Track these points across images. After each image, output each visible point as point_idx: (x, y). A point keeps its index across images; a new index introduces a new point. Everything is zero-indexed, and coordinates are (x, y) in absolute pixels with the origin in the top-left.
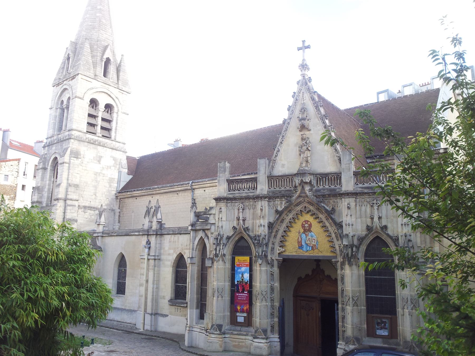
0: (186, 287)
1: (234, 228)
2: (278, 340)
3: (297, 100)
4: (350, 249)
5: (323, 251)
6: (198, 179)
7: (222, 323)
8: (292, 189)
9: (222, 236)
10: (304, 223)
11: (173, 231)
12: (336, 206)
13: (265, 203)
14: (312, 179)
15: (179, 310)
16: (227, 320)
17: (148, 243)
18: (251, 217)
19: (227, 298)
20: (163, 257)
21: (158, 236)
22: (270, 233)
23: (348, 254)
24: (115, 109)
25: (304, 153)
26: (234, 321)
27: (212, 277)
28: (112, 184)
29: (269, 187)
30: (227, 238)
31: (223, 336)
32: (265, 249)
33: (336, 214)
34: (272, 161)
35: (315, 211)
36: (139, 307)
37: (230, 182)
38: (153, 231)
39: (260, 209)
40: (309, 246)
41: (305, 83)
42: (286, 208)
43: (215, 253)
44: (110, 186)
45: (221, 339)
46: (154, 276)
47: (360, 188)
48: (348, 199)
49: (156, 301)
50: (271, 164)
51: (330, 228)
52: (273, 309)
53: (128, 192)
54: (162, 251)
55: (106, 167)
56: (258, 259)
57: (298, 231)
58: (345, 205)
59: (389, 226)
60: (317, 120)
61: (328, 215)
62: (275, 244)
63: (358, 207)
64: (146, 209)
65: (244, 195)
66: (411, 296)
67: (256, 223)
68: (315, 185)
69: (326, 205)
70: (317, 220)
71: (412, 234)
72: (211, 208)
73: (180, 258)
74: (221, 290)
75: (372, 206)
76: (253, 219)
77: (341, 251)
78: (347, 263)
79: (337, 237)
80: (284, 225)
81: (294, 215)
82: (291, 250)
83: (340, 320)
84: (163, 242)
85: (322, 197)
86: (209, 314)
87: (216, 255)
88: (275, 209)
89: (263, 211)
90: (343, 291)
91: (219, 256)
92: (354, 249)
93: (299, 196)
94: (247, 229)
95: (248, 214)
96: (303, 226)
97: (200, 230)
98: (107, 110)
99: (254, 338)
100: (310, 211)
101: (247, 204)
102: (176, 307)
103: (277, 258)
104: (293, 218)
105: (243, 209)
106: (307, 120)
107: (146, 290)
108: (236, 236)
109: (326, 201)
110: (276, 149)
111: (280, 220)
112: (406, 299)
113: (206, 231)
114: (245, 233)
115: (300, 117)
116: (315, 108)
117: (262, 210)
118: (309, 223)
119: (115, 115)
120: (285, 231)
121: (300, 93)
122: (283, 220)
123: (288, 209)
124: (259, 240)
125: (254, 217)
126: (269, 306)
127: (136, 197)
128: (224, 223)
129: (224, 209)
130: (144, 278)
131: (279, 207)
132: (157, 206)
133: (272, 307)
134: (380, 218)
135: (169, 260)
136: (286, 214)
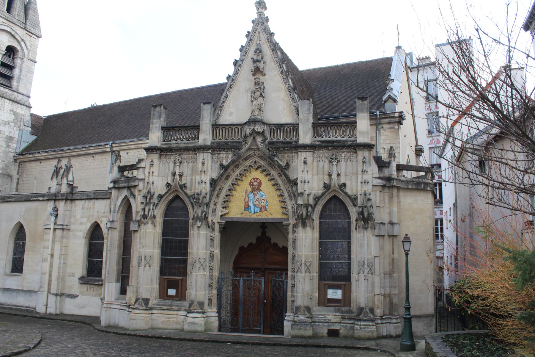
0: (102, 262)
1: (168, 185)
2: (217, 315)
3: (251, 40)
4: (305, 209)
5: (274, 212)
6: (120, 139)
7: (148, 297)
8: (241, 140)
9: (152, 194)
10: (253, 181)
11: (87, 195)
12: (291, 161)
13: (207, 156)
14: (266, 129)
17: (56, 209)
18: (190, 172)
20: (72, 227)
22: (213, 191)
23: (302, 215)
24: (20, 54)
25: (257, 99)
26: (163, 295)
28: (10, 144)
29: (213, 137)
30: (158, 196)
31: (150, 312)
32: (205, 209)
33: (291, 169)
34: (217, 108)
35: (267, 167)
36: (41, 287)
37: (165, 129)
38: (63, 195)
40: (258, 208)
41: (261, 23)
42: (233, 162)
43: (143, 213)
44: (8, 146)
45: (147, 315)
46: (61, 250)
47: (318, 141)
48: (305, 153)
49: (62, 279)
50: (217, 111)
51: (282, 187)
52: (212, 279)
53: (30, 154)
54: (72, 220)
55: (4, 122)
56: (196, 221)
57: (245, 190)
58: (301, 160)
59: (348, 184)
60: (273, 64)
63: (315, 163)
64: (54, 169)
66: (368, 259)
67: (195, 179)
68: (268, 136)
69: (280, 160)
70: (269, 177)
71: (372, 193)
73: (96, 227)
74: (149, 259)
75: (331, 162)
76: (192, 174)
77: (294, 212)
78: (300, 225)
79: (290, 196)
80: (229, 182)
81: (241, 171)
82: (236, 211)
84: (73, 209)
85: (276, 148)
86: (133, 286)
87: (145, 217)
88: (219, 163)
89: (206, 165)
91: (148, 217)
92: (310, 209)
93: (250, 149)
95: (186, 168)
96: (251, 184)
97: (124, 188)
98: (8, 54)
99: (188, 313)
101: (186, 156)
102: (89, 286)
103: (219, 221)
105: (181, 163)
106: (262, 62)
107: (51, 266)
108: (170, 195)
109: (280, 156)
110: (224, 94)
111: (225, 176)
112: (362, 262)
113: (132, 190)
114: (181, 191)
115: (255, 58)
117: (203, 163)
118: (258, 181)
119: (18, 61)
121: (255, 33)
122: (229, 176)
123: (234, 164)
124: (199, 199)
125: (194, 171)
127: (40, 160)
129: (156, 162)
131: (224, 161)
133: (211, 277)
134: (339, 175)
135: (81, 231)
136: (233, 169)
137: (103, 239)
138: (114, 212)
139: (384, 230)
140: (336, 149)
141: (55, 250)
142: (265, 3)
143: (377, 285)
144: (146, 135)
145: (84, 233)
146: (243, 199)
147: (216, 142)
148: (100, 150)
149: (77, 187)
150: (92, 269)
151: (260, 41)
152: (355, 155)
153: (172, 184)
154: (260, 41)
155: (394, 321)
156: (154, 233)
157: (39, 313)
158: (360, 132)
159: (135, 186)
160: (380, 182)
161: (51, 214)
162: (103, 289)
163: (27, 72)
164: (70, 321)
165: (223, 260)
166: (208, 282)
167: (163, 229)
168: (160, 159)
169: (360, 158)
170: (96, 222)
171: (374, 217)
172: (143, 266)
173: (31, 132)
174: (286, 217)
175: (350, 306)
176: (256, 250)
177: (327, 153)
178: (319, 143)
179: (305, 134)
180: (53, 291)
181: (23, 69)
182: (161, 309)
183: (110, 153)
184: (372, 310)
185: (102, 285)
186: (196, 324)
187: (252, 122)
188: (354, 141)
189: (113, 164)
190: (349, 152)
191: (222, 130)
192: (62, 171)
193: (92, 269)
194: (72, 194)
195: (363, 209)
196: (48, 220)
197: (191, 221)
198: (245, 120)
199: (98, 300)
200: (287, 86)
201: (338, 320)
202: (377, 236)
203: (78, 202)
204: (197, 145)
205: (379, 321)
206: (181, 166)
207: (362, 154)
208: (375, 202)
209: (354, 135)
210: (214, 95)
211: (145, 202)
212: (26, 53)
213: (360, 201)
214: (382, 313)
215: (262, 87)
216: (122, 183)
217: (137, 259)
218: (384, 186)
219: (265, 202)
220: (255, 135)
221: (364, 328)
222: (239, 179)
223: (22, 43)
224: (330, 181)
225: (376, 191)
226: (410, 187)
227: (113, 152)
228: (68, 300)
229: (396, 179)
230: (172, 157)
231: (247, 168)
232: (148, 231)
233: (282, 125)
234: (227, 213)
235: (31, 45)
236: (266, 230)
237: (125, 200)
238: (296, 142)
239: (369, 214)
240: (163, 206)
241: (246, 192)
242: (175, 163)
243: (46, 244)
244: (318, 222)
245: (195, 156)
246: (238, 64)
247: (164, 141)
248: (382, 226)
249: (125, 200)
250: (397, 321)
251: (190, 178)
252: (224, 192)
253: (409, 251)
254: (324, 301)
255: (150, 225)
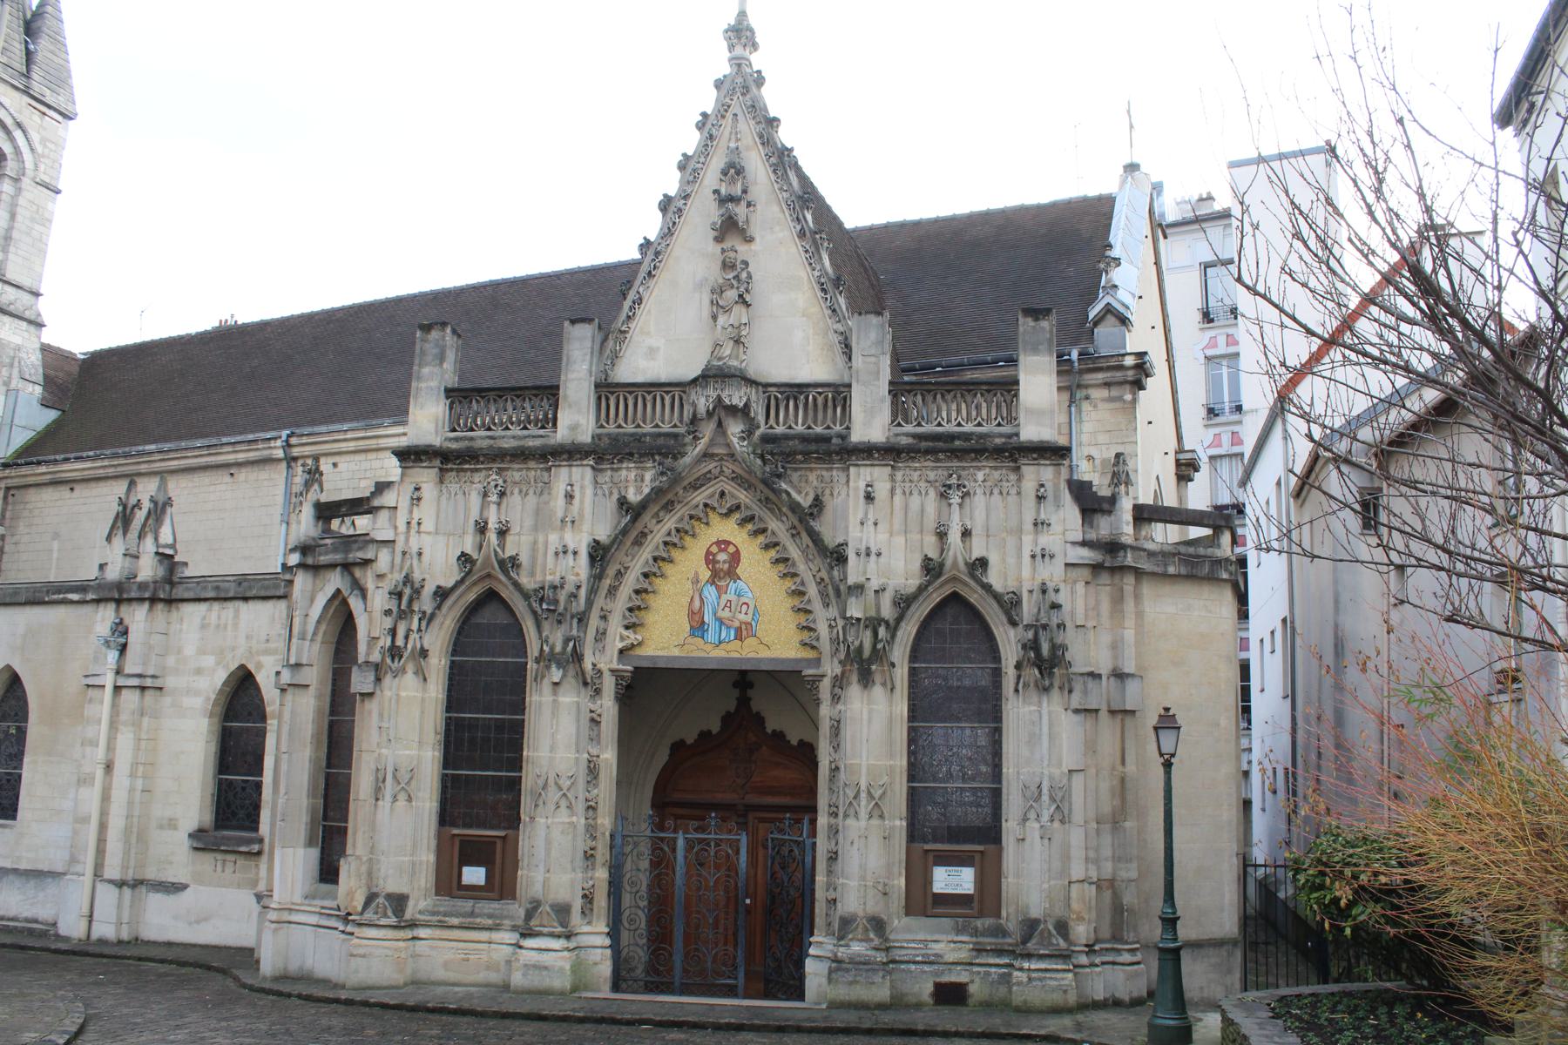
0: (258, 786)
1: (464, 558)
2: (608, 942)
3: (711, 137)
4: (869, 633)
5: (776, 640)
6: (313, 423)
7: (404, 890)
8: (682, 430)
9: (417, 585)
10: (714, 549)
11: (217, 588)
12: (827, 492)
13: (580, 475)
14: (753, 397)
15: (230, 866)
16: (425, 878)
17: (121, 629)
18: (529, 522)
19: (428, 805)
20: (170, 682)
21: (160, 606)
22: (597, 577)
23: (860, 649)
26: (448, 884)
27: (374, 732)
30: (435, 593)
32: (574, 632)
34: (611, 336)
35: (757, 510)
36: (73, 860)
37: (456, 395)
38: (143, 586)
39: (562, 493)
40: (728, 627)
41: (741, 90)
42: (657, 492)
43: (389, 643)
46: (137, 749)
47: (907, 435)
48: (869, 469)
50: (610, 343)
51: (801, 567)
53: (39, 463)
54: (171, 661)
56: (548, 667)
57: (691, 576)
58: (856, 489)
59: (994, 559)
60: (776, 208)
61: (801, 521)
62: (610, 618)
64: (115, 508)
65: (507, 444)
66: (1051, 778)
68: (761, 418)
69: (794, 487)
70: (761, 539)
71: (1062, 586)
72: (381, 487)
73: (242, 687)
75: (943, 496)
76: (535, 528)
77: (835, 641)
78: (854, 678)
79: (823, 595)
80: (646, 553)
82: (666, 639)
83: (821, 866)
85: (783, 454)
86: (359, 858)
87: (395, 652)
88: (616, 496)
89: (576, 501)
90: (835, 770)
91: (406, 655)
92: (882, 632)
93: (706, 455)
94: (510, 565)
95: (518, 510)
96: (710, 559)
97: (333, 566)
99: (524, 936)
100: (738, 507)
101: (517, 476)
102: (219, 856)
103: (615, 666)
104: (678, 531)
105: (502, 494)
106: (744, 204)
107: (106, 797)
109: (795, 476)
110: (632, 295)
112: (1034, 788)
113: (358, 573)
116: (770, 171)
117: (569, 497)
118: (731, 549)
120: (646, 575)
122: (644, 535)
123: (662, 499)
124: (556, 602)
125: (541, 521)
126: (581, 829)
127: (71, 483)
128: (427, 542)
129: (429, 491)
130: (100, 753)
132: (161, 499)
134: (966, 534)
135: (197, 693)
136: (657, 514)
137: (263, 718)
138: (303, 638)
139: (1098, 695)
140: (960, 459)
141: (118, 751)
142: (752, 31)
143: (1077, 853)
144: (399, 412)
145: (208, 699)
146: (685, 601)
147: (608, 435)
148: (252, 455)
149: (186, 564)
150: (228, 805)
151: (738, 140)
152: (1013, 477)
153: (475, 557)
154: (738, 140)
155: (1127, 957)
156: (423, 700)
157: (67, 939)
158: (1030, 411)
159: (366, 563)
160: (1086, 555)
161: (107, 642)
162: (263, 867)
163: (33, 220)
164: (162, 961)
165: (625, 780)
166: (582, 846)
167: (449, 690)
168: (441, 482)
169: (1029, 485)
170: (242, 667)
171: (1068, 656)
172: (388, 798)
173: (43, 398)
174: (811, 654)
175: (998, 916)
176: (722, 754)
177: (933, 468)
178: (910, 440)
179: (870, 413)
180: (112, 871)
181: (19, 210)
182: (443, 926)
183: (284, 464)
184: (1062, 928)
185: (259, 853)
186: (546, 968)
187: (715, 376)
188: (1010, 436)
189: (292, 503)
190: (996, 468)
191: (626, 399)
192: (140, 516)
193: (228, 805)
194: (172, 584)
195: (1036, 634)
196: (96, 659)
197: (531, 666)
198: (694, 371)
199: (246, 898)
200: (817, 273)
201: (963, 955)
202: (1077, 711)
203: (188, 609)
204: (552, 442)
205: (1084, 960)
206: (504, 505)
207: (1036, 474)
208: (1073, 613)
209: (1012, 419)
210: (602, 296)
211: (395, 609)
212: (29, 164)
213: (1028, 610)
214: (1092, 935)
215: (744, 275)
216: (326, 553)
217: (372, 778)
218: (1096, 568)
219: (751, 612)
220: (723, 414)
221: (1040, 979)
222: (675, 545)
223: (18, 134)
224: (942, 551)
225: (1075, 582)
226: (1171, 570)
227: (291, 460)
228: (155, 900)
229: (1132, 548)
230: (477, 477)
231: (699, 512)
232: (403, 694)
233: (801, 388)
234: (640, 644)
235: (44, 141)
236: (750, 693)
237: (336, 603)
238: (843, 437)
239: (1054, 647)
240: (448, 622)
241: (696, 581)
242: (485, 495)
243: (90, 732)
244: (906, 670)
245: (546, 474)
246: (672, 208)
247: (454, 430)
248: (1091, 683)
249: (336, 603)
250: (1135, 959)
251: (531, 538)
252: (631, 581)
253: (1173, 755)
254: (922, 902)
255: (410, 678)
